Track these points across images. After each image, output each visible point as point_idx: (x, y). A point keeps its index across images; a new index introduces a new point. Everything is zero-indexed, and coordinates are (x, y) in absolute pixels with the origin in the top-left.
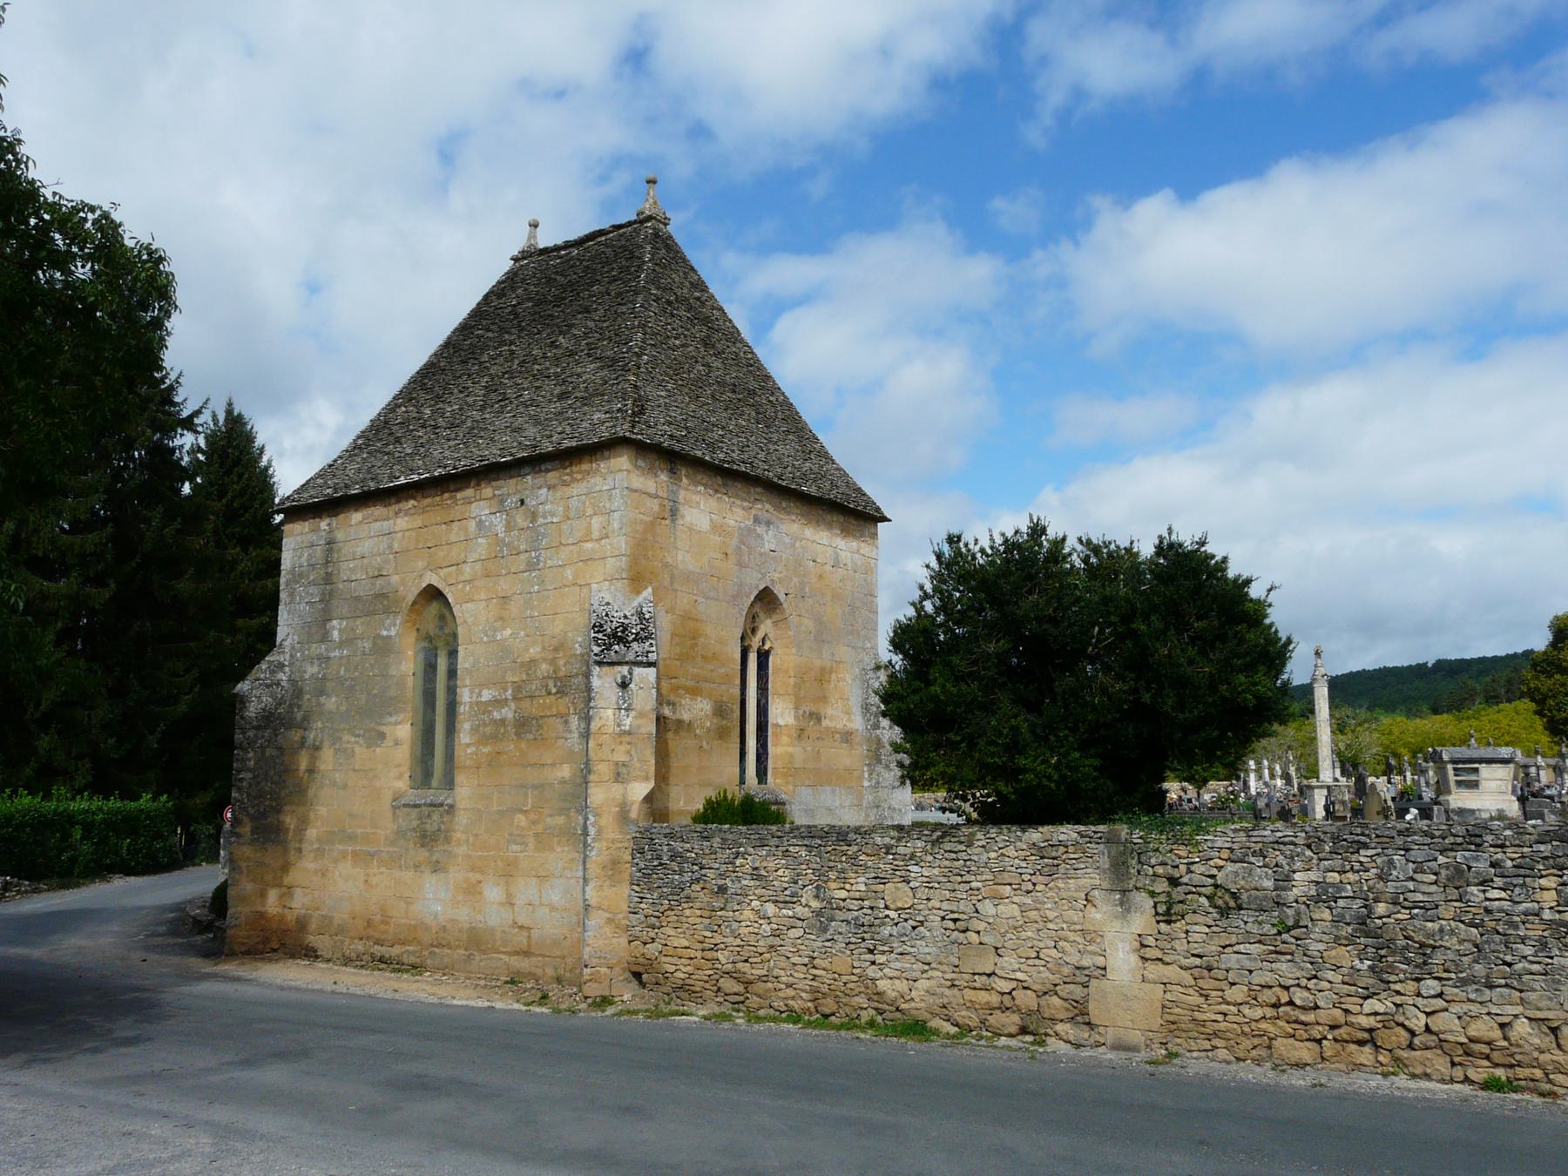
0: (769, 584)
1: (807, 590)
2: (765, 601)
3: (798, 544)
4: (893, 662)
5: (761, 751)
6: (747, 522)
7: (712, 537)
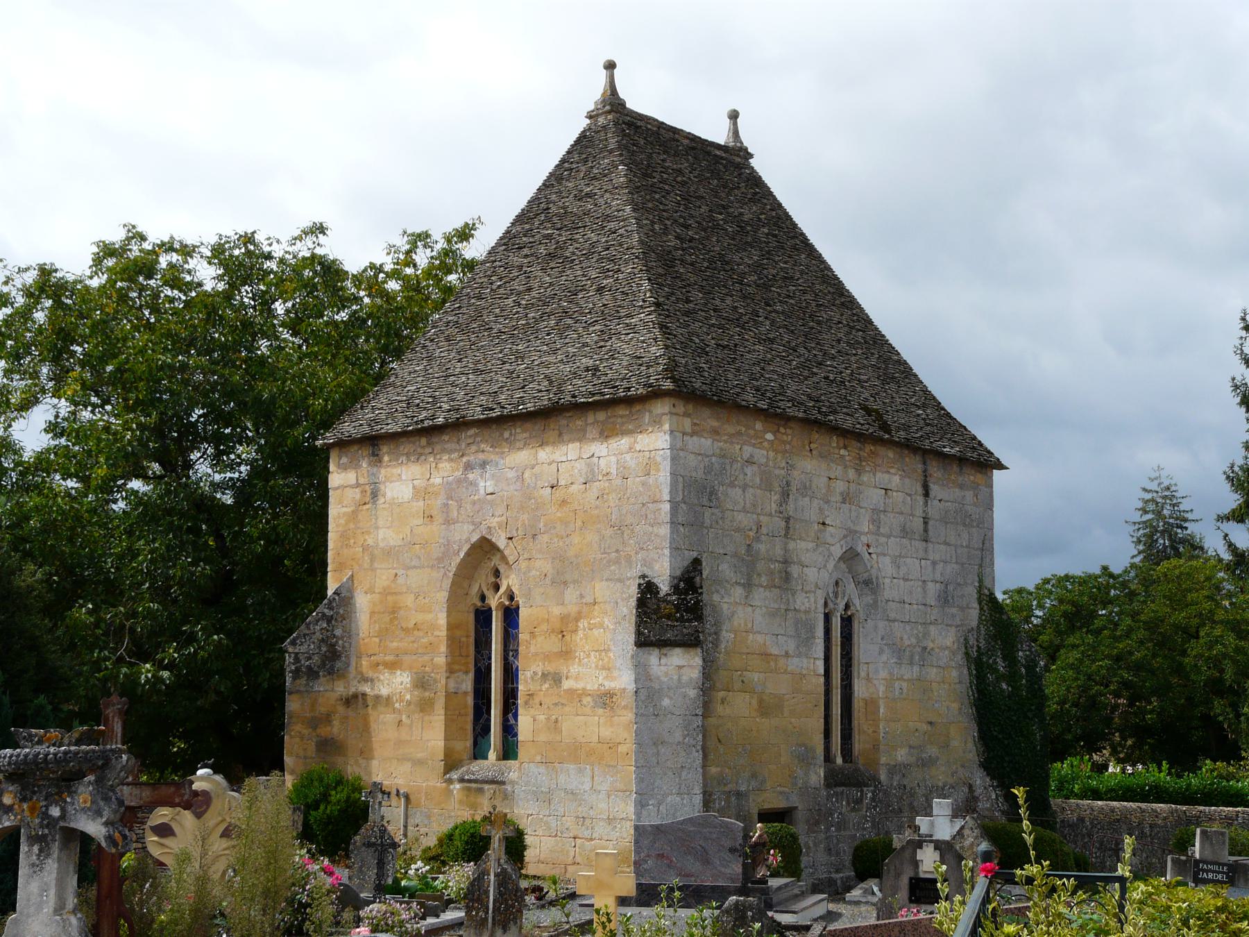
7: (415, 504)
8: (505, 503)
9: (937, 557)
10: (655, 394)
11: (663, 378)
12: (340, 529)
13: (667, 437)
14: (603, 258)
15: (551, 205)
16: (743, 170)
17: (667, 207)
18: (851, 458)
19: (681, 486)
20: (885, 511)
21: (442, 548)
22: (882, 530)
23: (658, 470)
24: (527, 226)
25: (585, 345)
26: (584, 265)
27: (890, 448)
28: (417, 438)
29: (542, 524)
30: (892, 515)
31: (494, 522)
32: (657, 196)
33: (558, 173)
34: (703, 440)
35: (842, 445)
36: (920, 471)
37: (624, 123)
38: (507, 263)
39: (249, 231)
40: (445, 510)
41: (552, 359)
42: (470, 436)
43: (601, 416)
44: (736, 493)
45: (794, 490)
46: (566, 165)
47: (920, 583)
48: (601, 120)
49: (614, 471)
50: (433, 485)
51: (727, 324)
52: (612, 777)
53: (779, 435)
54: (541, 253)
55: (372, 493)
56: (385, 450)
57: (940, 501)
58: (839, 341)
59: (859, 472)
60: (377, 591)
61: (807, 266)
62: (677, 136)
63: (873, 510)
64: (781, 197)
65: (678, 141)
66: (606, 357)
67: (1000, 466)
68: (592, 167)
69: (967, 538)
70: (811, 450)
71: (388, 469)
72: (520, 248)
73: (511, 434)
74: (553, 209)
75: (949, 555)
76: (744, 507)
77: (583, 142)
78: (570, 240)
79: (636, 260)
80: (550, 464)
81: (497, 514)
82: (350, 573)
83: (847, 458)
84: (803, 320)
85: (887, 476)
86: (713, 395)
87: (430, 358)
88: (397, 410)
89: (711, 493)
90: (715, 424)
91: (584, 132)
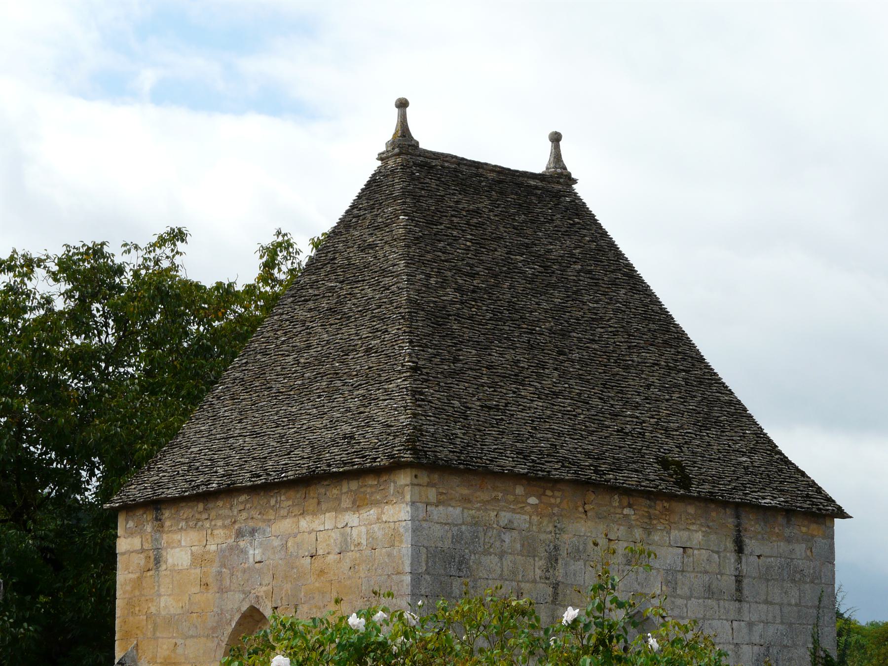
7: (193, 571)
8: (271, 572)
9: (754, 618)
10: (396, 466)
11: (404, 449)
12: (127, 596)
13: (409, 509)
14: (375, 317)
15: (337, 255)
16: (562, 199)
17: (451, 256)
18: (638, 517)
19: (424, 557)
20: (683, 571)
21: (216, 617)
22: (679, 592)
23: (401, 542)
24: (314, 277)
25: (348, 410)
26: (358, 323)
27: (690, 504)
28: (195, 503)
29: (303, 594)
30: (693, 575)
31: (262, 591)
32: (441, 245)
33: (347, 219)
34: (450, 509)
35: (626, 504)
36: (731, 526)
37: (415, 164)
38: (293, 317)
39: (99, 242)
40: (219, 578)
41: (318, 424)
42: (242, 503)
43: (354, 485)
44: (491, 561)
45: (564, 554)
46: (355, 211)
47: (732, 647)
48: (391, 163)
49: (364, 542)
50: (208, 552)
51: (501, 381)
53: (544, 498)
54: (323, 308)
55: (155, 559)
56: (166, 515)
57: (759, 557)
58: (648, 387)
59: (648, 532)
60: (159, 661)
61: (626, 304)
62: (481, 170)
63: (667, 571)
64: (605, 225)
65: (481, 175)
66: (363, 424)
67: (841, 514)
68: (377, 215)
69: (797, 596)
70: (586, 511)
71: (170, 535)
72: (306, 301)
73: (276, 502)
74: (339, 261)
75: (770, 615)
76: (501, 575)
77: (373, 186)
78: (350, 294)
79: (402, 321)
80: (310, 533)
81: (264, 583)
82: (135, 642)
83: (633, 517)
84: (605, 366)
85: (685, 534)
86: (460, 464)
87: (215, 418)
88: (178, 474)
89: (460, 563)
90: (466, 491)
91: (374, 175)
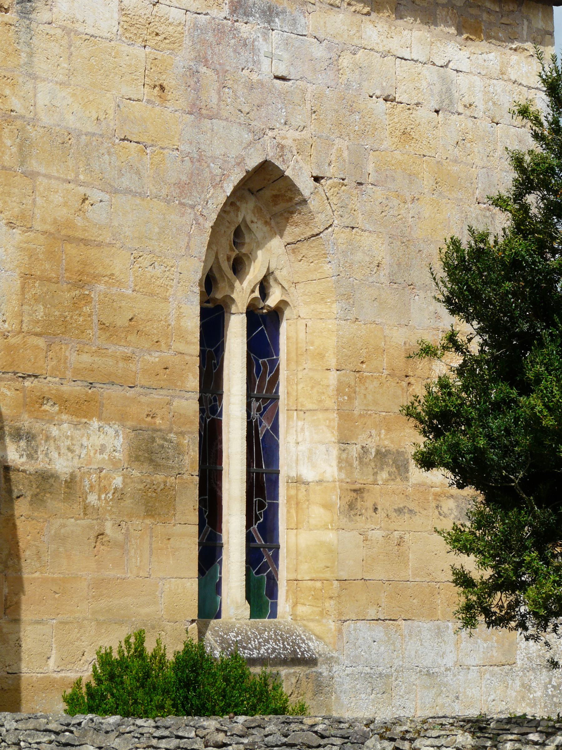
0: (272, 155)
1: (371, 168)
2: (268, 193)
3: (346, 61)
4: (461, 338)
5: (260, 541)
6: (214, 12)
7: (125, 48)
49: (481, 106)
52: (486, 640)
